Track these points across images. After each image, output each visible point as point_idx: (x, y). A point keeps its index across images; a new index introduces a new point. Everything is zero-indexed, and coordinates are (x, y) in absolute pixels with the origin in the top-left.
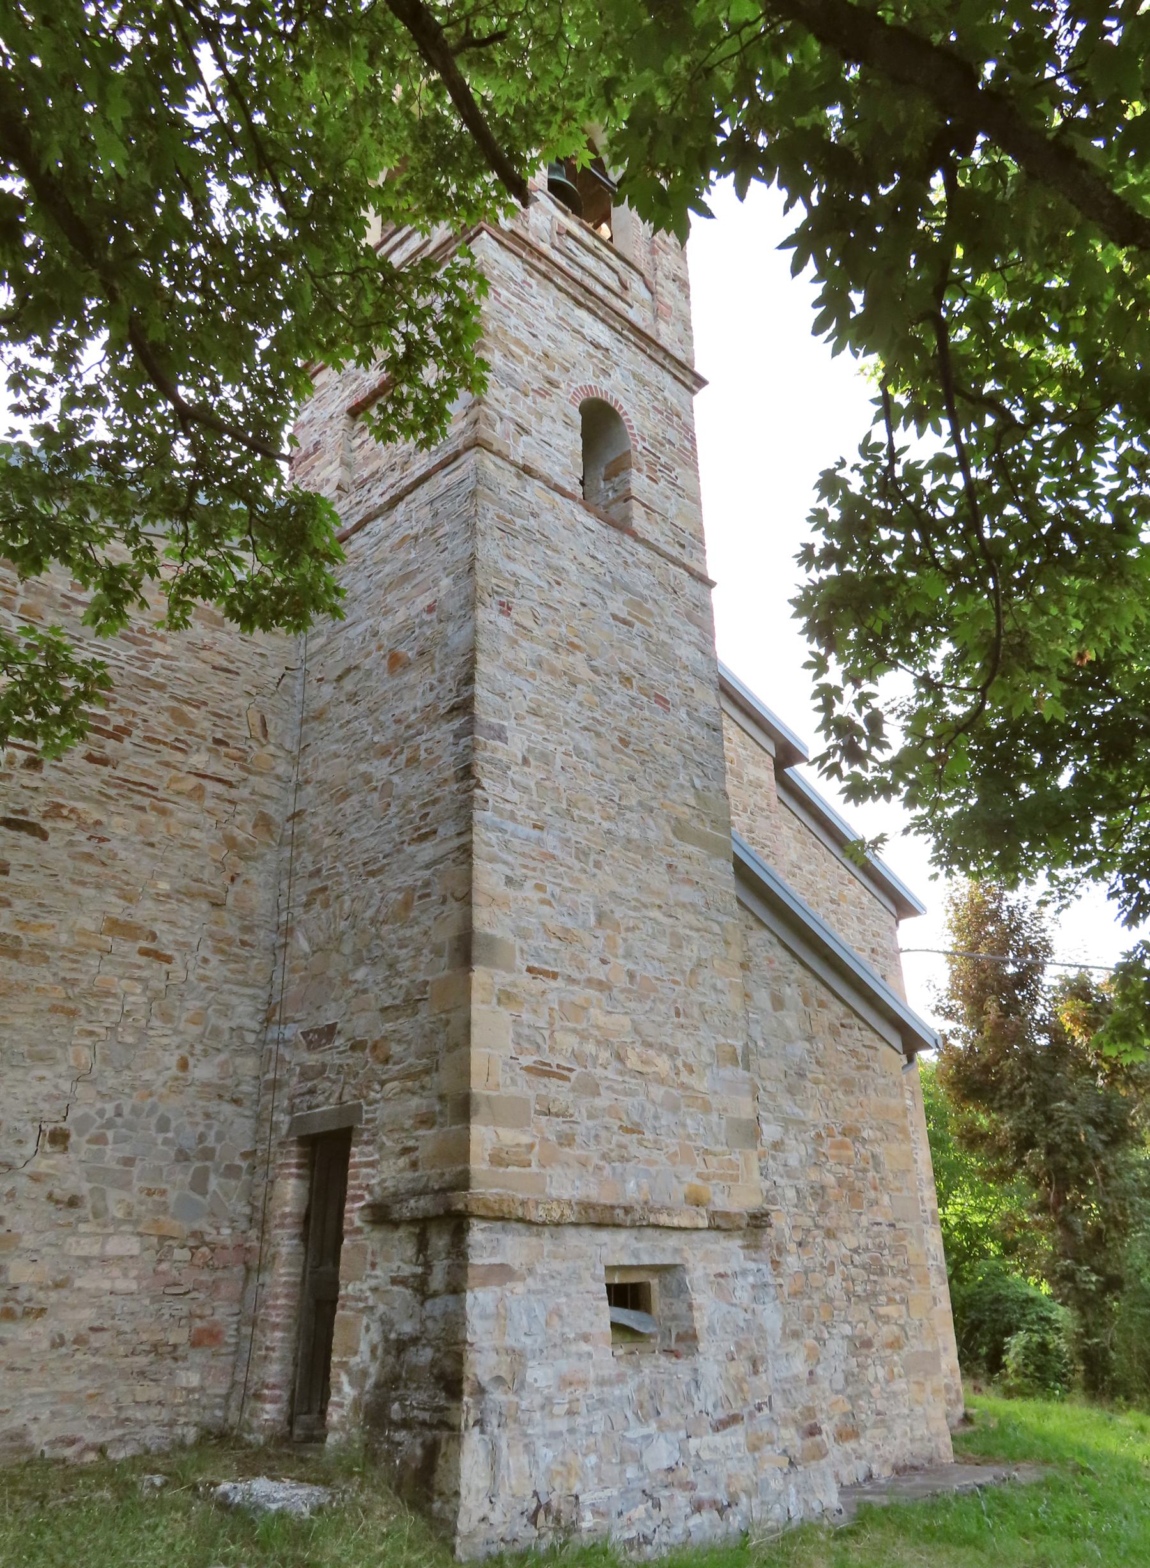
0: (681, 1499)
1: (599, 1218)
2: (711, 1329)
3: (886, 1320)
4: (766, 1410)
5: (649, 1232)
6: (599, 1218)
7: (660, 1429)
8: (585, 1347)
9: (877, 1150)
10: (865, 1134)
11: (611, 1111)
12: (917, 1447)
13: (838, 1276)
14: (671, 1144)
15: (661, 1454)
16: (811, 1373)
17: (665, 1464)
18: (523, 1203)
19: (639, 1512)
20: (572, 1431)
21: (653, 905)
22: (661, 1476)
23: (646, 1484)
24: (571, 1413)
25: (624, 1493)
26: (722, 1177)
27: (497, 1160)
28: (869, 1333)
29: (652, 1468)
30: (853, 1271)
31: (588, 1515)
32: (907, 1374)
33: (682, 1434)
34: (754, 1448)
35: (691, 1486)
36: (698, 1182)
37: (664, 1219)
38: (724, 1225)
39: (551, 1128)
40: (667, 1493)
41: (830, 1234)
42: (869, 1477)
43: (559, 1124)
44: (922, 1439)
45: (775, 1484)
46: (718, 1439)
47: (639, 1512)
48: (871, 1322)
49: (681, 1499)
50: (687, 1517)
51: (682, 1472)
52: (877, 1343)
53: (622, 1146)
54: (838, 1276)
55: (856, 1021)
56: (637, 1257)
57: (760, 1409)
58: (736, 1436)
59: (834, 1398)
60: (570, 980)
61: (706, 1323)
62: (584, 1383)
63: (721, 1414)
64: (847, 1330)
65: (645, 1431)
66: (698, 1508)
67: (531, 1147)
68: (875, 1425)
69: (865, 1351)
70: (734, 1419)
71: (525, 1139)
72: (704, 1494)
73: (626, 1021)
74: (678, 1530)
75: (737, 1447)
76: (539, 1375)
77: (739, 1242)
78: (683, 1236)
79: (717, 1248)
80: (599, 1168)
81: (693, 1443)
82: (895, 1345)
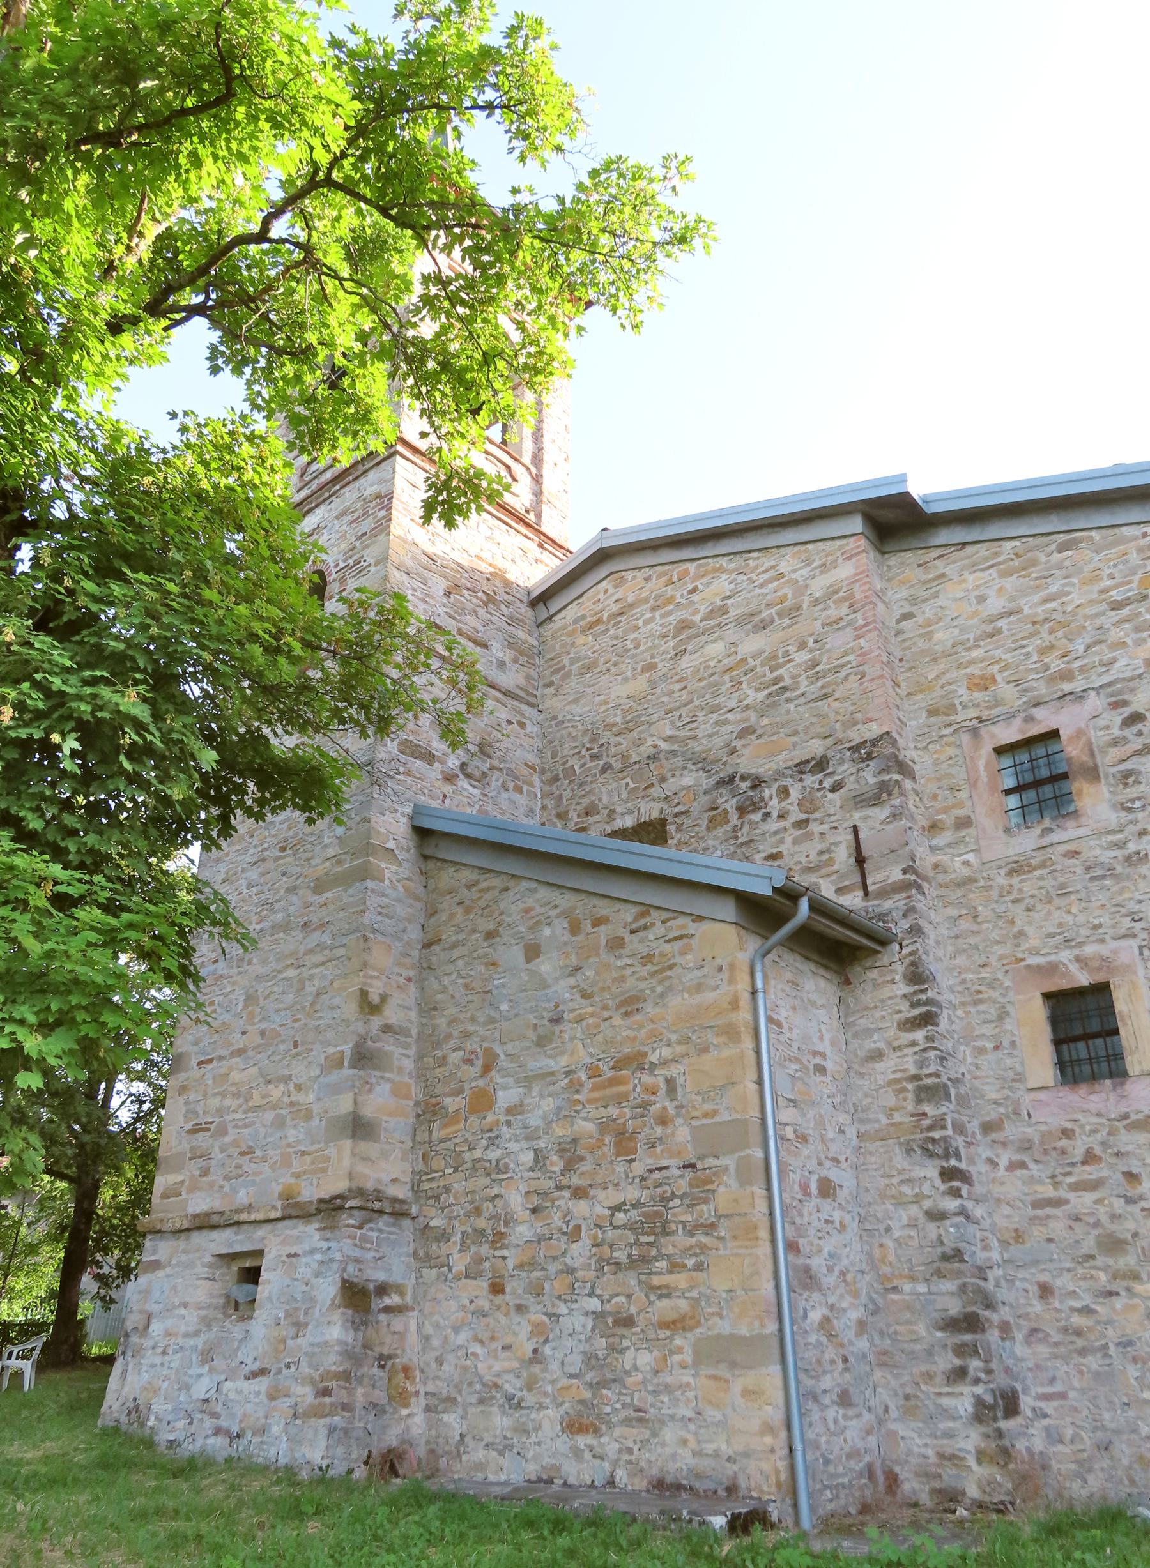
0: (209, 1424)
1: (205, 1223)
2: (269, 1298)
3: (665, 1292)
4: (293, 1369)
5: (245, 1227)
6: (205, 1223)
7: (210, 1371)
8: (183, 1311)
9: (674, 1071)
10: (654, 1058)
11: (235, 1143)
12: (705, 1464)
13: (585, 1241)
14: (274, 1154)
15: (202, 1388)
16: (535, 1351)
17: (202, 1396)
18: (162, 1221)
19: (181, 1424)
20: (162, 1365)
21: (287, 967)
22: (199, 1404)
23: (190, 1407)
24: (164, 1353)
25: (176, 1410)
26: (313, 1172)
27: (165, 1196)
28: (633, 1310)
29: (195, 1397)
30: (611, 1234)
31: (152, 1418)
32: (697, 1363)
33: (223, 1377)
34: (272, 1397)
35: (215, 1415)
36: (292, 1180)
37: (244, 1217)
38: (294, 1213)
39: (194, 1167)
40: (199, 1416)
41: (579, 1193)
42: (611, 1483)
43: (200, 1163)
44: (716, 1454)
45: (275, 1430)
46: (245, 1386)
47: (181, 1424)
48: (639, 1294)
49: (209, 1424)
50: (207, 1437)
51: (213, 1404)
52: (641, 1321)
53: (239, 1167)
54: (585, 1241)
55: (655, 914)
56: (231, 1246)
57: (288, 1366)
58: (262, 1385)
59: (565, 1382)
60: (221, 1058)
61: (266, 1294)
62: (176, 1335)
63: (256, 1367)
64: (594, 1304)
65: (199, 1371)
66: (217, 1431)
67: (182, 1182)
68: (627, 1422)
69: (621, 1331)
70: (263, 1372)
71: (180, 1178)
72: (224, 1423)
73: (255, 1070)
74: (199, 1443)
75: (258, 1393)
76: (156, 1328)
77: (317, 1225)
78: (269, 1227)
79: (295, 1232)
80: (222, 1187)
81: (227, 1385)
82: (676, 1325)
